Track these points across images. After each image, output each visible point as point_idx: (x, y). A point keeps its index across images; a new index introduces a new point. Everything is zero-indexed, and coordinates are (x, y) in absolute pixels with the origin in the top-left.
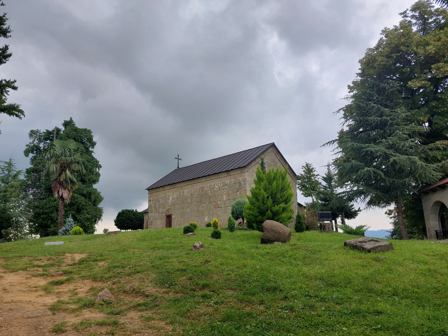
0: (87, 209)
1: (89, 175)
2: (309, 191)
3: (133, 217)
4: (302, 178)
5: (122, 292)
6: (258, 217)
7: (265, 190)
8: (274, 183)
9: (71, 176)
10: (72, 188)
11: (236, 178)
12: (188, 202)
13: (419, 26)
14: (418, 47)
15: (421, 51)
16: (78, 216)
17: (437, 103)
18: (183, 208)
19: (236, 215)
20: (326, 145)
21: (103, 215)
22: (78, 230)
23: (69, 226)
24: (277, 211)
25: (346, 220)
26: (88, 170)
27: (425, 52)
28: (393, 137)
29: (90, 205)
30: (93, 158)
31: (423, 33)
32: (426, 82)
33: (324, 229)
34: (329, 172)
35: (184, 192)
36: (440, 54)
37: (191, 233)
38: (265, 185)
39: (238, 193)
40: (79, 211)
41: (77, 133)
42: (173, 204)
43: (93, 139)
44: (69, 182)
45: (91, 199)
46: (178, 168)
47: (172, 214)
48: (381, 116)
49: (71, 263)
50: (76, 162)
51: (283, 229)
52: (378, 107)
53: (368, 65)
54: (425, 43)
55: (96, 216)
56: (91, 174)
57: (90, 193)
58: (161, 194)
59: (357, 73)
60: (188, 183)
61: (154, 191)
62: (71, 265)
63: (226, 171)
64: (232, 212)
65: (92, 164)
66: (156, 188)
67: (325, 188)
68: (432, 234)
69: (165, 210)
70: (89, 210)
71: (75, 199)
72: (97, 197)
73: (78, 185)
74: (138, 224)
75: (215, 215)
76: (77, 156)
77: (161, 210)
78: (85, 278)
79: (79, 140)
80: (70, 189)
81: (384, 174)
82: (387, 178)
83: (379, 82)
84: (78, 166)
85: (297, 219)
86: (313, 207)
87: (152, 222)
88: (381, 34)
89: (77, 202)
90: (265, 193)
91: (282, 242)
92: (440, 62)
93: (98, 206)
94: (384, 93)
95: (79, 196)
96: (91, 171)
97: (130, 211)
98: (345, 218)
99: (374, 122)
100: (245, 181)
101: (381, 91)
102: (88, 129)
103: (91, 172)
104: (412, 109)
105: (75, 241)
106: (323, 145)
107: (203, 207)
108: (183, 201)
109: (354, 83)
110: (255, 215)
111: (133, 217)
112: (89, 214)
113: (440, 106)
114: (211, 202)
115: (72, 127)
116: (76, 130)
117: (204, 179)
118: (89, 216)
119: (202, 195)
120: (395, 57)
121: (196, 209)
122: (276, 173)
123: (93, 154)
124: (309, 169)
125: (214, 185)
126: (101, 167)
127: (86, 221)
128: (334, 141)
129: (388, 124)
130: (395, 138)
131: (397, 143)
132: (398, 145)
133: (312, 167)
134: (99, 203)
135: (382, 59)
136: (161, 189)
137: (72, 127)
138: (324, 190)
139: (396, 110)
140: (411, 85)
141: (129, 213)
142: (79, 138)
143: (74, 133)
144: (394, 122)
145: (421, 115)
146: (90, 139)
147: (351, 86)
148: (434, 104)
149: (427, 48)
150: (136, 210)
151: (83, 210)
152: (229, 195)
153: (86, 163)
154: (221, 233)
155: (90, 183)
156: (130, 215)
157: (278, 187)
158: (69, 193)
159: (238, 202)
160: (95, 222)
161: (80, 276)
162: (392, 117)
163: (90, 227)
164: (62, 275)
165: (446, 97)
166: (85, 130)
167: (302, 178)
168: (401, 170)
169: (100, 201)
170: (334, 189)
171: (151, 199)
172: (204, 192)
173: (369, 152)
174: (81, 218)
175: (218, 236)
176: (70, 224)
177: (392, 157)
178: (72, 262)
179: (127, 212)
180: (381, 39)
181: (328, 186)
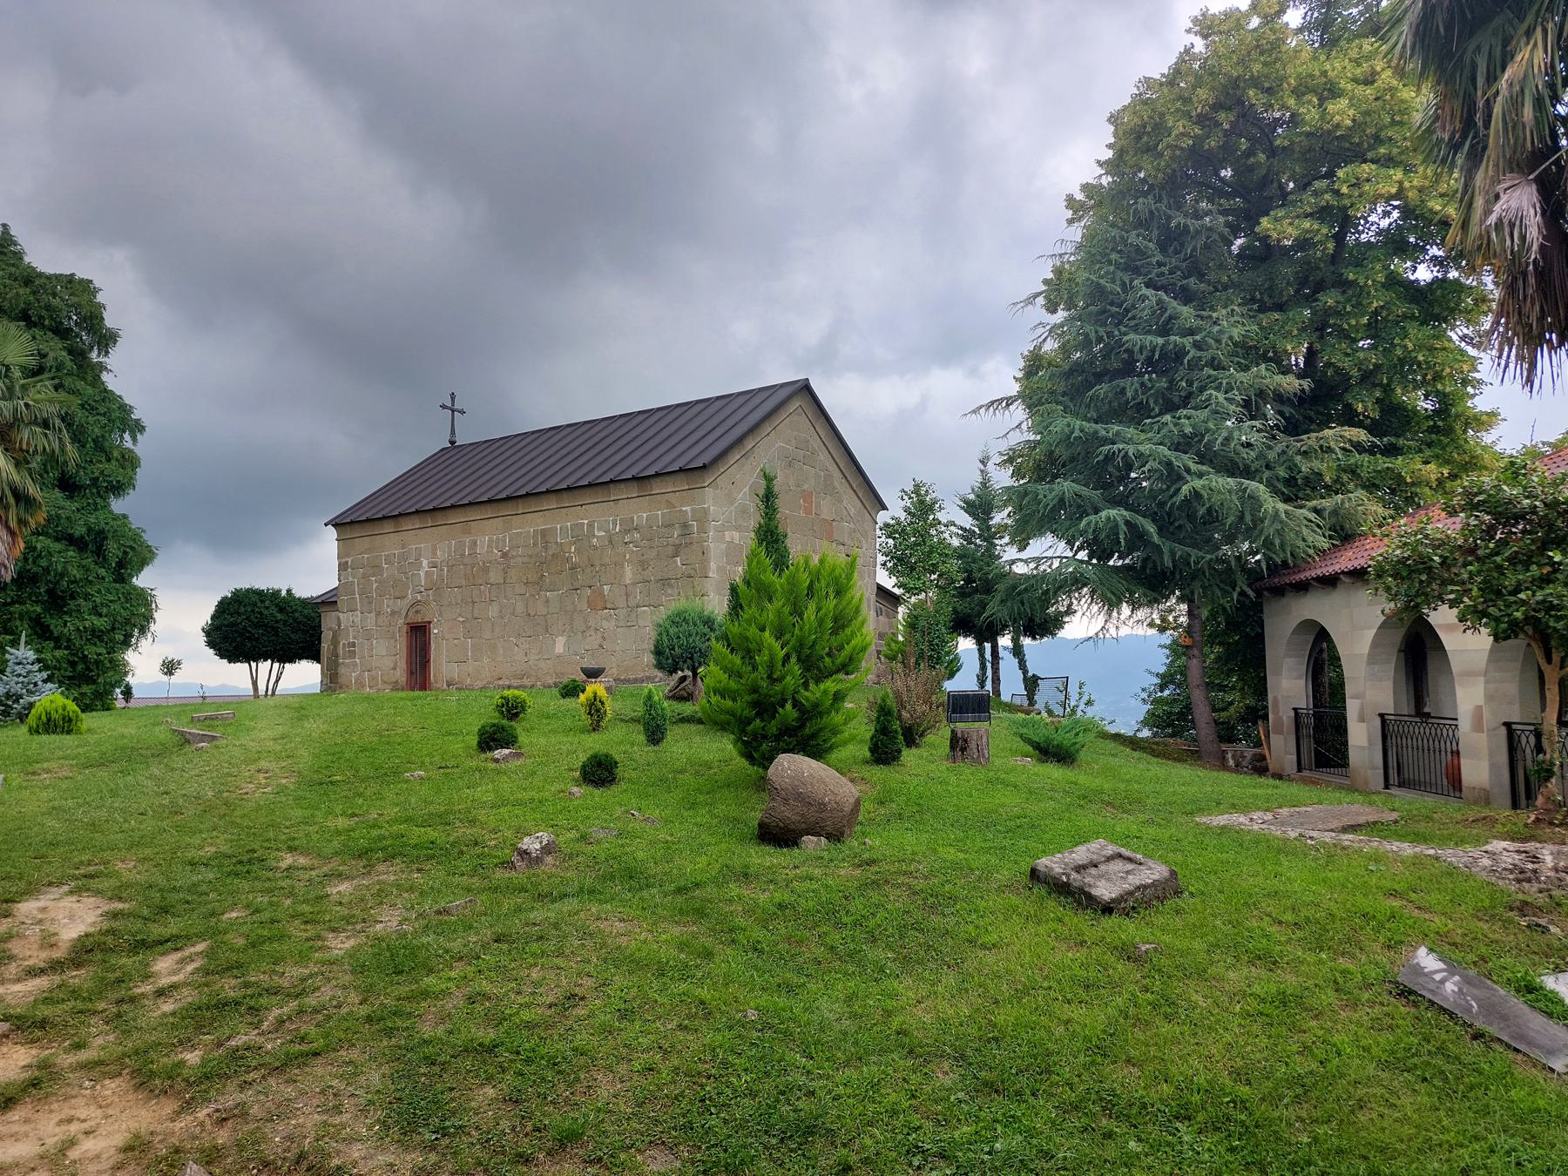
0: (92, 595)
1: (91, 461)
2: (919, 579)
3: (279, 616)
4: (896, 531)
5: (254, 1168)
6: (749, 724)
7: (779, 634)
8: (810, 613)
9: (16, 478)
10: (22, 522)
11: (670, 505)
12: (492, 581)
13: (1310, 10)
14: (1304, 94)
15: (1310, 114)
16: (55, 624)
17: (1341, 299)
18: (473, 602)
19: (670, 661)
20: (983, 410)
21: (156, 615)
22: (60, 711)
23: (21, 679)
24: (816, 705)
25: (1026, 641)
26: (90, 445)
27: (1322, 118)
28: (1196, 408)
29: (103, 578)
30: (107, 395)
31: (1322, 36)
32: (1316, 227)
33: (963, 750)
34: (985, 484)
35: (475, 543)
36: (1368, 131)
37: (507, 751)
38: (779, 613)
39: (678, 559)
40: (58, 601)
41: (34, 293)
42: (435, 587)
43: (103, 319)
44: (12, 500)
45: (104, 557)
46: (452, 443)
47: (430, 622)
48: (1164, 331)
49: (39, 958)
50: (35, 423)
51: (836, 792)
52: (1160, 299)
53: (1139, 138)
54: (1325, 84)
55: (127, 621)
56: (103, 459)
57: (102, 532)
58: (389, 544)
59: (1098, 162)
60: (489, 512)
61: (357, 531)
62: (43, 971)
63: (634, 478)
64: (656, 647)
65: (103, 420)
66: (368, 520)
67: (967, 535)
68: (1284, 718)
69: (402, 605)
70: (98, 600)
71: (39, 556)
72: (132, 548)
73: (48, 499)
74: (298, 643)
75: (593, 633)
76: (38, 396)
77: (388, 605)
78: (102, 1068)
79: (47, 322)
80: (13, 524)
81: (1160, 531)
82: (1168, 543)
83: (1170, 209)
84: (46, 435)
85: (878, 718)
86: (929, 634)
87: (353, 645)
88: (1189, 31)
89: (47, 570)
90: (777, 645)
91: (829, 837)
92: (1365, 161)
93: (134, 580)
94: (1182, 245)
95: (57, 546)
96: (102, 448)
97: (266, 595)
98: (1025, 635)
99: (1141, 349)
100: (703, 517)
101: (1171, 239)
102: (80, 275)
103: (102, 450)
104: (1263, 309)
105: (48, 771)
106: (974, 412)
107: (547, 601)
108: (474, 578)
109: (1086, 188)
110: (739, 714)
111: (279, 616)
112: (101, 615)
113: (1348, 309)
114: (576, 585)
115: (13, 265)
116: (30, 278)
117: (552, 503)
118: (101, 623)
119: (543, 560)
120: (1226, 126)
121: (520, 608)
122: (818, 573)
123: (105, 377)
124: (922, 502)
125: (591, 525)
126: (142, 429)
127: (87, 639)
128: (1009, 401)
129: (1186, 361)
130: (1202, 414)
131: (1208, 430)
132: (1210, 438)
133: (934, 495)
134: (140, 570)
135: (1184, 127)
136: (388, 527)
137: (13, 265)
138: (965, 543)
139: (1215, 315)
140: (1268, 230)
141: (262, 602)
142: (44, 313)
143: (21, 291)
144: (1206, 355)
145: (1287, 335)
146: (93, 319)
147: (1078, 199)
148: (1330, 302)
149: (1331, 107)
150: (289, 591)
151: (75, 599)
152: (643, 565)
153: (80, 416)
154: (616, 763)
155: (98, 493)
156: (267, 608)
157: (821, 622)
158: (13, 541)
159: (679, 615)
160: (126, 643)
161: (84, 1055)
162: (1198, 338)
163: (108, 665)
164: (7, 1037)
165: (1370, 282)
166: (70, 282)
167: (896, 531)
168: (1212, 517)
169: (143, 563)
170: (997, 542)
171: (350, 560)
172: (553, 549)
173: (1119, 459)
174: (66, 630)
175: (606, 773)
176: (23, 672)
177: (1189, 478)
178: (44, 955)
179: (255, 598)
180: (1187, 51)
181: (977, 530)
